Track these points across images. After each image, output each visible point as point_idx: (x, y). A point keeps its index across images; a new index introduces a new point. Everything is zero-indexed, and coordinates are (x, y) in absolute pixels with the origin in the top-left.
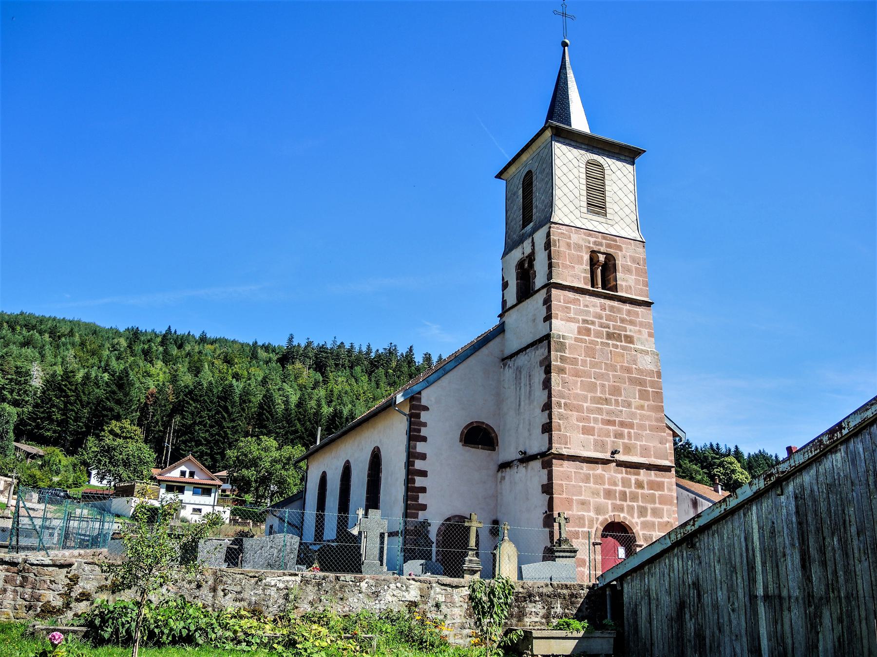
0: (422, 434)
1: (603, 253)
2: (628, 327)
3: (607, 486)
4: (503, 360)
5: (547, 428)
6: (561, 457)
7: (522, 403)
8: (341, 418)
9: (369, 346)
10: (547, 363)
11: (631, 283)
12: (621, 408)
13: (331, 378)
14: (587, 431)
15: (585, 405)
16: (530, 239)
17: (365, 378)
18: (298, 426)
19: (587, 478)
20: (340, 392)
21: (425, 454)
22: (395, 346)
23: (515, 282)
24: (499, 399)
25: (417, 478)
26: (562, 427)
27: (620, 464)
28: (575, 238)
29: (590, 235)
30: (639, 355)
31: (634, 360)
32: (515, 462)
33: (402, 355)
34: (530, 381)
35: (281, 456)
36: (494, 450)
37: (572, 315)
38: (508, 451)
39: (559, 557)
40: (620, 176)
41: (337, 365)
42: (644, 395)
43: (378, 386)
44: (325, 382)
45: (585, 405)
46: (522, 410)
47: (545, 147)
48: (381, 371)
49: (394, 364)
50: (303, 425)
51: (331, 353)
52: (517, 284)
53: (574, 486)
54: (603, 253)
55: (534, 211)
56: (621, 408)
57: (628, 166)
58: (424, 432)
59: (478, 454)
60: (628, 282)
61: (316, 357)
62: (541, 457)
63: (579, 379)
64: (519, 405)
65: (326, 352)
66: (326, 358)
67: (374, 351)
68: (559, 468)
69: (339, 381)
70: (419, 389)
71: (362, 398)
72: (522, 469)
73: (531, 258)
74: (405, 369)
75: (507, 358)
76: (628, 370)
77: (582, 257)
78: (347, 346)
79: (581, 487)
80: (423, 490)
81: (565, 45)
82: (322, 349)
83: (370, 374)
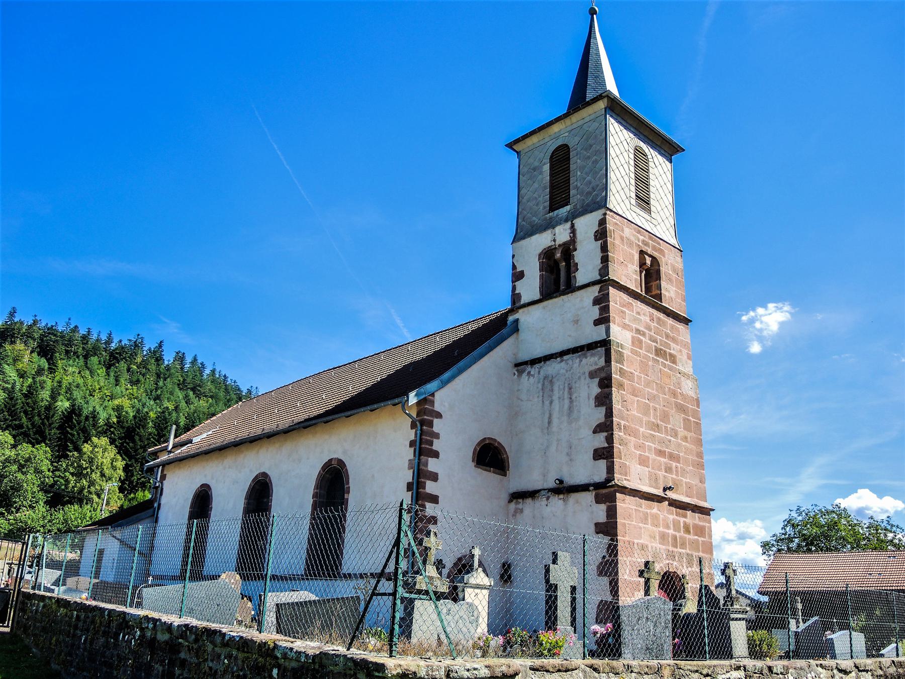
0: (434, 448)
1: (650, 256)
2: (673, 345)
3: (661, 529)
4: (517, 365)
5: (605, 454)
6: (624, 490)
7: (555, 421)
8: (80, 415)
9: (110, 335)
10: (603, 375)
11: (673, 294)
12: (669, 437)
13: (60, 366)
14: (643, 461)
15: (641, 430)
16: (568, 225)
17: (102, 371)
18: (24, 420)
19: (645, 519)
20: (70, 384)
21: (437, 474)
22: (142, 338)
23: (537, 274)
24: (514, 414)
25: (428, 505)
26: (623, 454)
27: (674, 504)
28: (628, 232)
29: (639, 232)
30: (683, 378)
31: (679, 384)
32: (543, 493)
33: (150, 349)
34: (570, 394)
35: (17, 455)
36: (505, 475)
37: (627, 322)
38: (518, 480)
39: (736, 619)
40: (661, 170)
41: (67, 352)
42: (687, 425)
43: (117, 382)
44: (52, 370)
45: (641, 430)
46: (554, 428)
47: (594, 120)
48: (123, 365)
49: (139, 360)
50: (30, 419)
51: (62, 337)
52: (541, 277)
53: (635, 527)
54: (650, 256)
55: (572, 192)
56: (669, 437)
57: (667, 162)
58: (437, 445)
59: (489, 477)
60: (672, 293)
61: (42, 340)
62: (595, 489)
63: (636, 399)
64: (549, 423)
65: (55, 335)
66: (56, 341)
67: (116, 341)
68: (624, 504)
69: (70, 372)
70: (433, 390)
71: (97, 395)
72: (556, 502)
73: (568, 249)
74: (153, 367)
75: (525, 363)
76: (674, 394)
77: (633, 256)
78: (83, 331)
79: (640, 528)
80: (434, 520)
81: (593, 12)
82: (51, 331)
83: (108, 368)
